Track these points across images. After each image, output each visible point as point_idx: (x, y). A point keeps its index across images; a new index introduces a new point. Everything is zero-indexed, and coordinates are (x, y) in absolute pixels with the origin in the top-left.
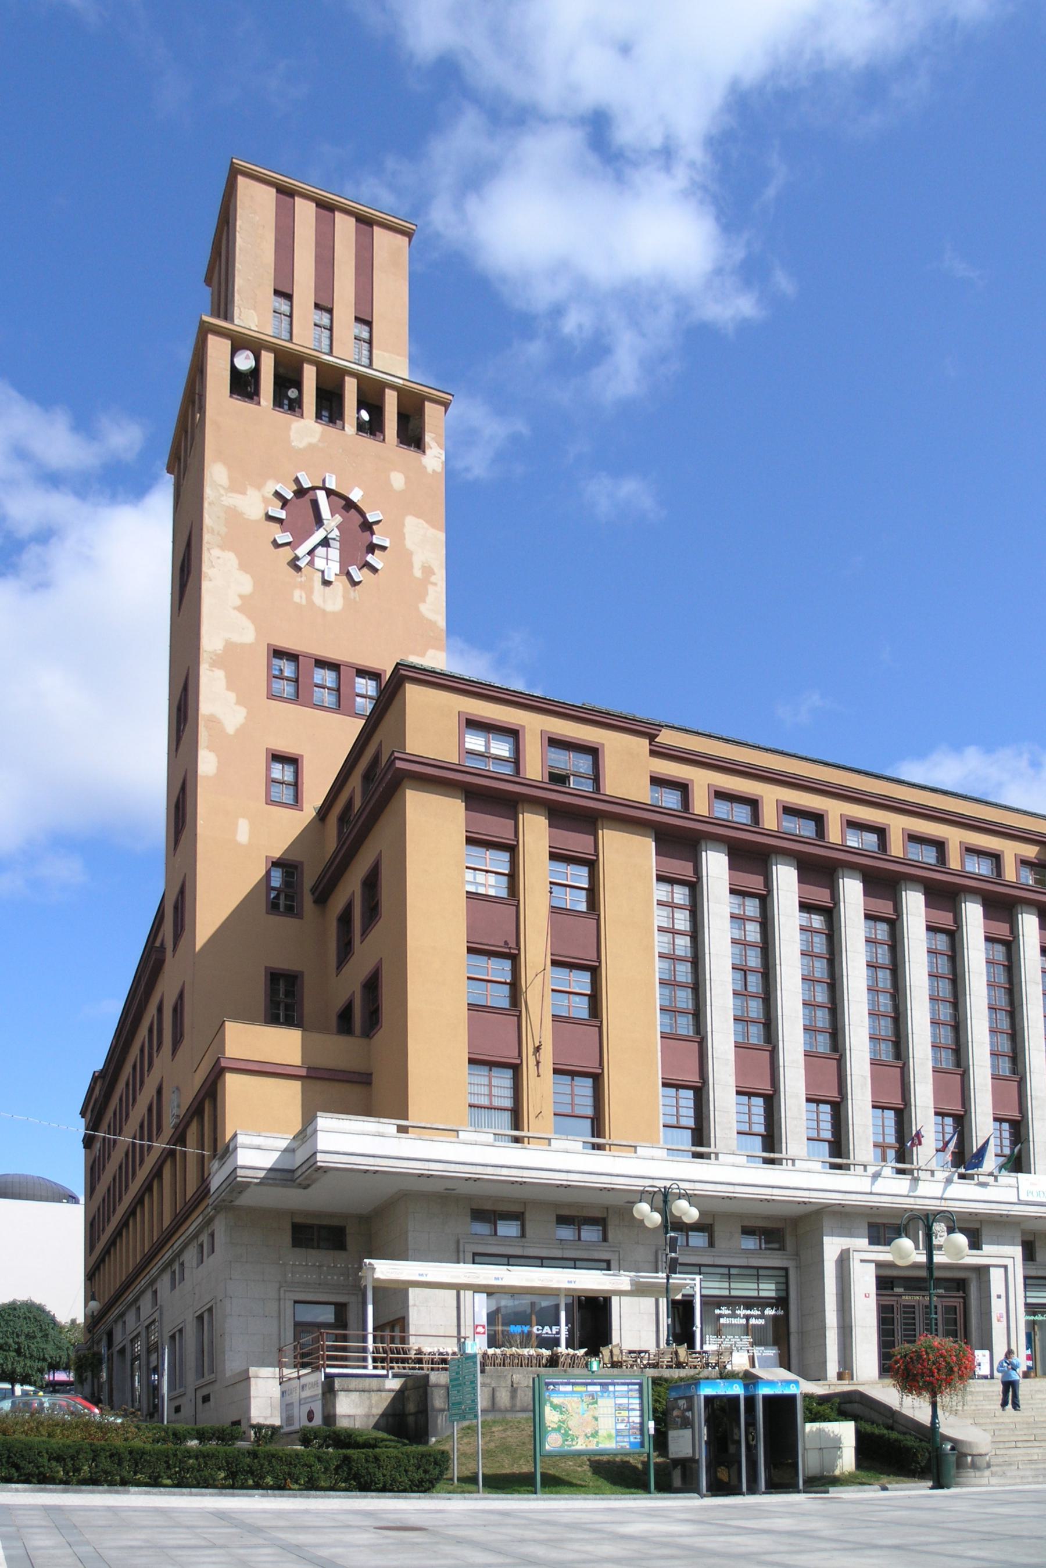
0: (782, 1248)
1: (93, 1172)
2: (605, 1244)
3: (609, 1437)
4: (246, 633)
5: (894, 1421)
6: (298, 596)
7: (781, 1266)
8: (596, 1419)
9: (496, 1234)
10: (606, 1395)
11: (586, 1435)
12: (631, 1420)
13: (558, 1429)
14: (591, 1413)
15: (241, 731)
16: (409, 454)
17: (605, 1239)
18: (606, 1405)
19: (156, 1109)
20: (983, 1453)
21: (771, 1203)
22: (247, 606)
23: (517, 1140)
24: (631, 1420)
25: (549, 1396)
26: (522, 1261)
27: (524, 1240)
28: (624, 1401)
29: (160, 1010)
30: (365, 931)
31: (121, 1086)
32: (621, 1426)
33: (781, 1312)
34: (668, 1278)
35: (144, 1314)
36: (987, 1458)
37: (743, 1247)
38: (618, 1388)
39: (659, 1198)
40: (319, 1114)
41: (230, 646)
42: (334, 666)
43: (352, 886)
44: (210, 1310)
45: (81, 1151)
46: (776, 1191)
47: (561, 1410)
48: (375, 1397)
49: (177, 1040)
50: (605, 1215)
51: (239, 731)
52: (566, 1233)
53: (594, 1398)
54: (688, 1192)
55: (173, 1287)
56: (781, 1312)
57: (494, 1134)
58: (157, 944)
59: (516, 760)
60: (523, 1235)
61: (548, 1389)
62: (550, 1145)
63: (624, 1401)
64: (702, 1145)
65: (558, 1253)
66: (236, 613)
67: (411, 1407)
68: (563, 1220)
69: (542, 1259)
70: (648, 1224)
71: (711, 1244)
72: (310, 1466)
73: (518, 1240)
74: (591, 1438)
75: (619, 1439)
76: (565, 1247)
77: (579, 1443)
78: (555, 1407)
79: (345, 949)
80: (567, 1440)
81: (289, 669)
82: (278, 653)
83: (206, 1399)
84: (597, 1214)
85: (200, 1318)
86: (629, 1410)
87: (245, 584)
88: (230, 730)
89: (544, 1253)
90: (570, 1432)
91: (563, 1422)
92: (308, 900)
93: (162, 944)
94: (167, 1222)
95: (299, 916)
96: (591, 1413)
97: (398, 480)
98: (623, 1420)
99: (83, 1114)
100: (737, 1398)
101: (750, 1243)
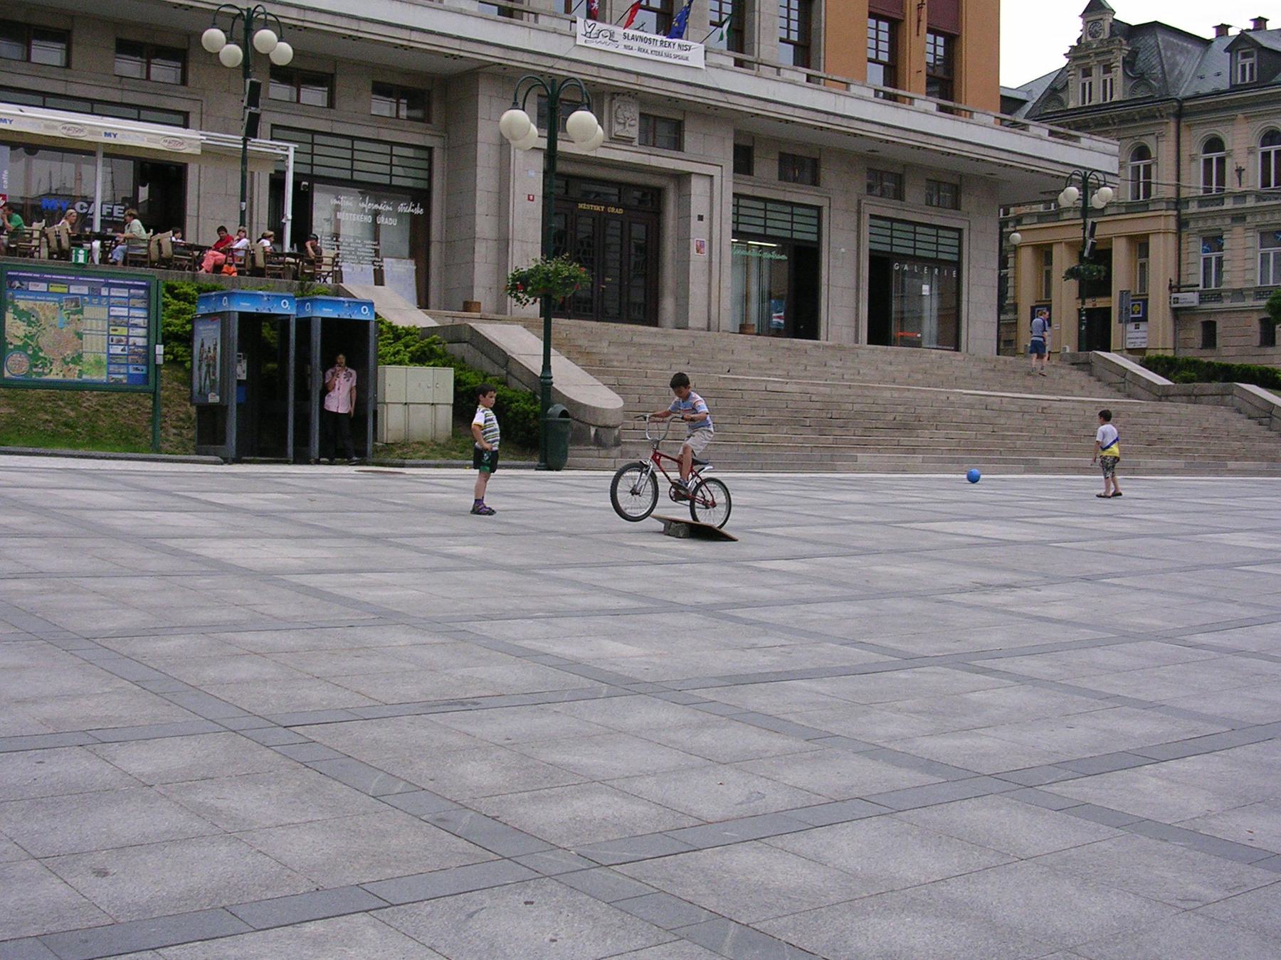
0: (426, 119)
2: (183, 88)
3: (98, 363)
5: (508, 373)
7: (423, 144)
8: (80, 336)
9: (28, 59)
10: (96, 301)
11: (64, 359)
12: (131, 340)
13: (22, 349)
14: (73, 327)
17: (184, 81)
18: (95, 318)
20: (611, 423)
21: (789, 125)
23: (894, 98)
24: (131, 340)
25: (13, 297)
26: (164, 116)
27: (67, 71)
28: (123, 312)
32: (117, 350)
33: (419, 211)
34: (245, 140)
36: (616, 432)
37: (373, 113)
38: (115, 292)
39: (240, 24)
46: (415, 36)
47: (29, 319)
50: (186, 47)
52: (129, 67)
53: (77, 305)
54: (281, 20)
56: (419, 211)
57: (996, 117)
60: (68, 65)
61: (11, 287)
62: (778, 74)
63: (123, 312)
64: (895, 86)
65: (115, 96)
68: (126, 47)
69: (92, 101)
71: (331, 104)
73: (61, 71)
74: (71, 366)
75: (112, 368)
76: (126, 87)
77: (54, 371)
78: (21, 314)
80: (36, 366)
84: (173, 42)
86: (129, 326)
89: (95, 94)
90: (41, 354)
91: (32, 337)
96: (73, 327)
98: (120, 341)
101: (383, 107)
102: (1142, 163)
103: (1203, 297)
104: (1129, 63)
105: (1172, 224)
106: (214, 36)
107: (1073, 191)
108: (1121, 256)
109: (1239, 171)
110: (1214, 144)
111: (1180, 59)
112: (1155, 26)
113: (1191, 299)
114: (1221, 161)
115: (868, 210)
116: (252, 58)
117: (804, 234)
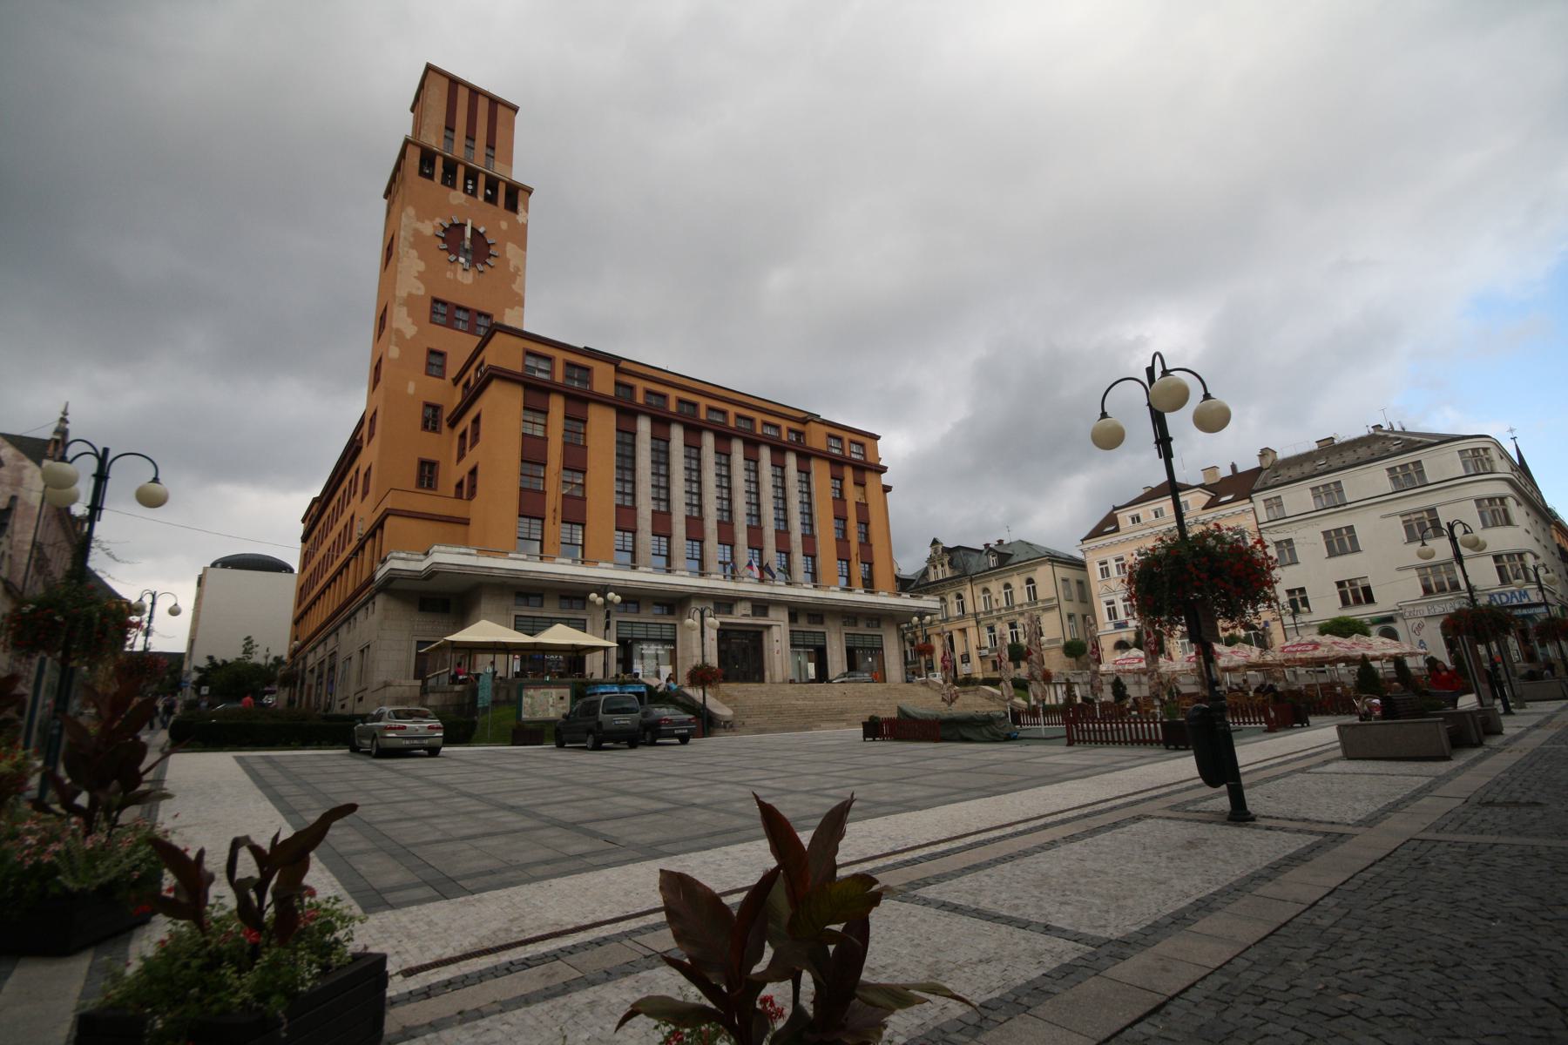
1: (306, 558)
4: (420, 290)
6: (449, 275)
15: (413, 338)
16: (511, 214)
19: (349, 526)
22: (421, 276)
29: (357, 472)
30: (472, 446)
31: (329, 510)
35: (329, 648)
40: (139, 734)
41: (410, 295)
42: (466, 310)
43: (467, 421)
44: (368, 647)
45: (299, 544)
48: (448, 695)
49: (365, 493)
51: (412, 338)
55: (349, 632)
58: (358, 438)
59: (551, 372)
66: (414, 280)
67: (467, 701)
70: (615, 601)
72: (1233, 855)
79: (461, 455)
81: (442, 310)
82: (436, 301)
83: (360, 699)
85: (362, 651)
87: (421, 266)
88: (408, 337)
92: (445, 425)
93: (361, 438)
94: (350, 592)
95: (440, 432)
97: (504, 225)
99: (303, 521)
100: (643, 693)
102: (1031, 586)
103: (990, 651)
104: (950, 563)
105: (975, 624)
106: (593, 596)
107: (916, 619)
108: (957, 637)
109: (997, 600)
110: (986, 590)
111: (970, 559)
112: (958, 548)
113: (985, 652)
114: (990, 597)
115: (844, 631)
116: (607, 603)
117: (819, 643)
